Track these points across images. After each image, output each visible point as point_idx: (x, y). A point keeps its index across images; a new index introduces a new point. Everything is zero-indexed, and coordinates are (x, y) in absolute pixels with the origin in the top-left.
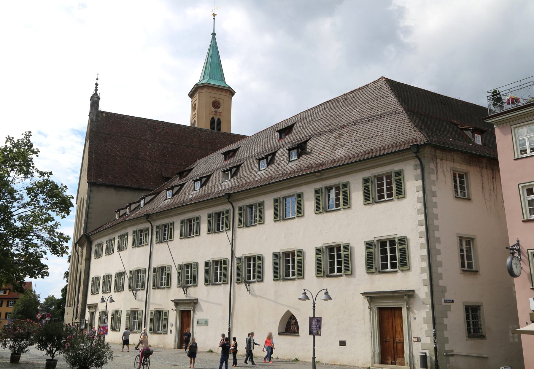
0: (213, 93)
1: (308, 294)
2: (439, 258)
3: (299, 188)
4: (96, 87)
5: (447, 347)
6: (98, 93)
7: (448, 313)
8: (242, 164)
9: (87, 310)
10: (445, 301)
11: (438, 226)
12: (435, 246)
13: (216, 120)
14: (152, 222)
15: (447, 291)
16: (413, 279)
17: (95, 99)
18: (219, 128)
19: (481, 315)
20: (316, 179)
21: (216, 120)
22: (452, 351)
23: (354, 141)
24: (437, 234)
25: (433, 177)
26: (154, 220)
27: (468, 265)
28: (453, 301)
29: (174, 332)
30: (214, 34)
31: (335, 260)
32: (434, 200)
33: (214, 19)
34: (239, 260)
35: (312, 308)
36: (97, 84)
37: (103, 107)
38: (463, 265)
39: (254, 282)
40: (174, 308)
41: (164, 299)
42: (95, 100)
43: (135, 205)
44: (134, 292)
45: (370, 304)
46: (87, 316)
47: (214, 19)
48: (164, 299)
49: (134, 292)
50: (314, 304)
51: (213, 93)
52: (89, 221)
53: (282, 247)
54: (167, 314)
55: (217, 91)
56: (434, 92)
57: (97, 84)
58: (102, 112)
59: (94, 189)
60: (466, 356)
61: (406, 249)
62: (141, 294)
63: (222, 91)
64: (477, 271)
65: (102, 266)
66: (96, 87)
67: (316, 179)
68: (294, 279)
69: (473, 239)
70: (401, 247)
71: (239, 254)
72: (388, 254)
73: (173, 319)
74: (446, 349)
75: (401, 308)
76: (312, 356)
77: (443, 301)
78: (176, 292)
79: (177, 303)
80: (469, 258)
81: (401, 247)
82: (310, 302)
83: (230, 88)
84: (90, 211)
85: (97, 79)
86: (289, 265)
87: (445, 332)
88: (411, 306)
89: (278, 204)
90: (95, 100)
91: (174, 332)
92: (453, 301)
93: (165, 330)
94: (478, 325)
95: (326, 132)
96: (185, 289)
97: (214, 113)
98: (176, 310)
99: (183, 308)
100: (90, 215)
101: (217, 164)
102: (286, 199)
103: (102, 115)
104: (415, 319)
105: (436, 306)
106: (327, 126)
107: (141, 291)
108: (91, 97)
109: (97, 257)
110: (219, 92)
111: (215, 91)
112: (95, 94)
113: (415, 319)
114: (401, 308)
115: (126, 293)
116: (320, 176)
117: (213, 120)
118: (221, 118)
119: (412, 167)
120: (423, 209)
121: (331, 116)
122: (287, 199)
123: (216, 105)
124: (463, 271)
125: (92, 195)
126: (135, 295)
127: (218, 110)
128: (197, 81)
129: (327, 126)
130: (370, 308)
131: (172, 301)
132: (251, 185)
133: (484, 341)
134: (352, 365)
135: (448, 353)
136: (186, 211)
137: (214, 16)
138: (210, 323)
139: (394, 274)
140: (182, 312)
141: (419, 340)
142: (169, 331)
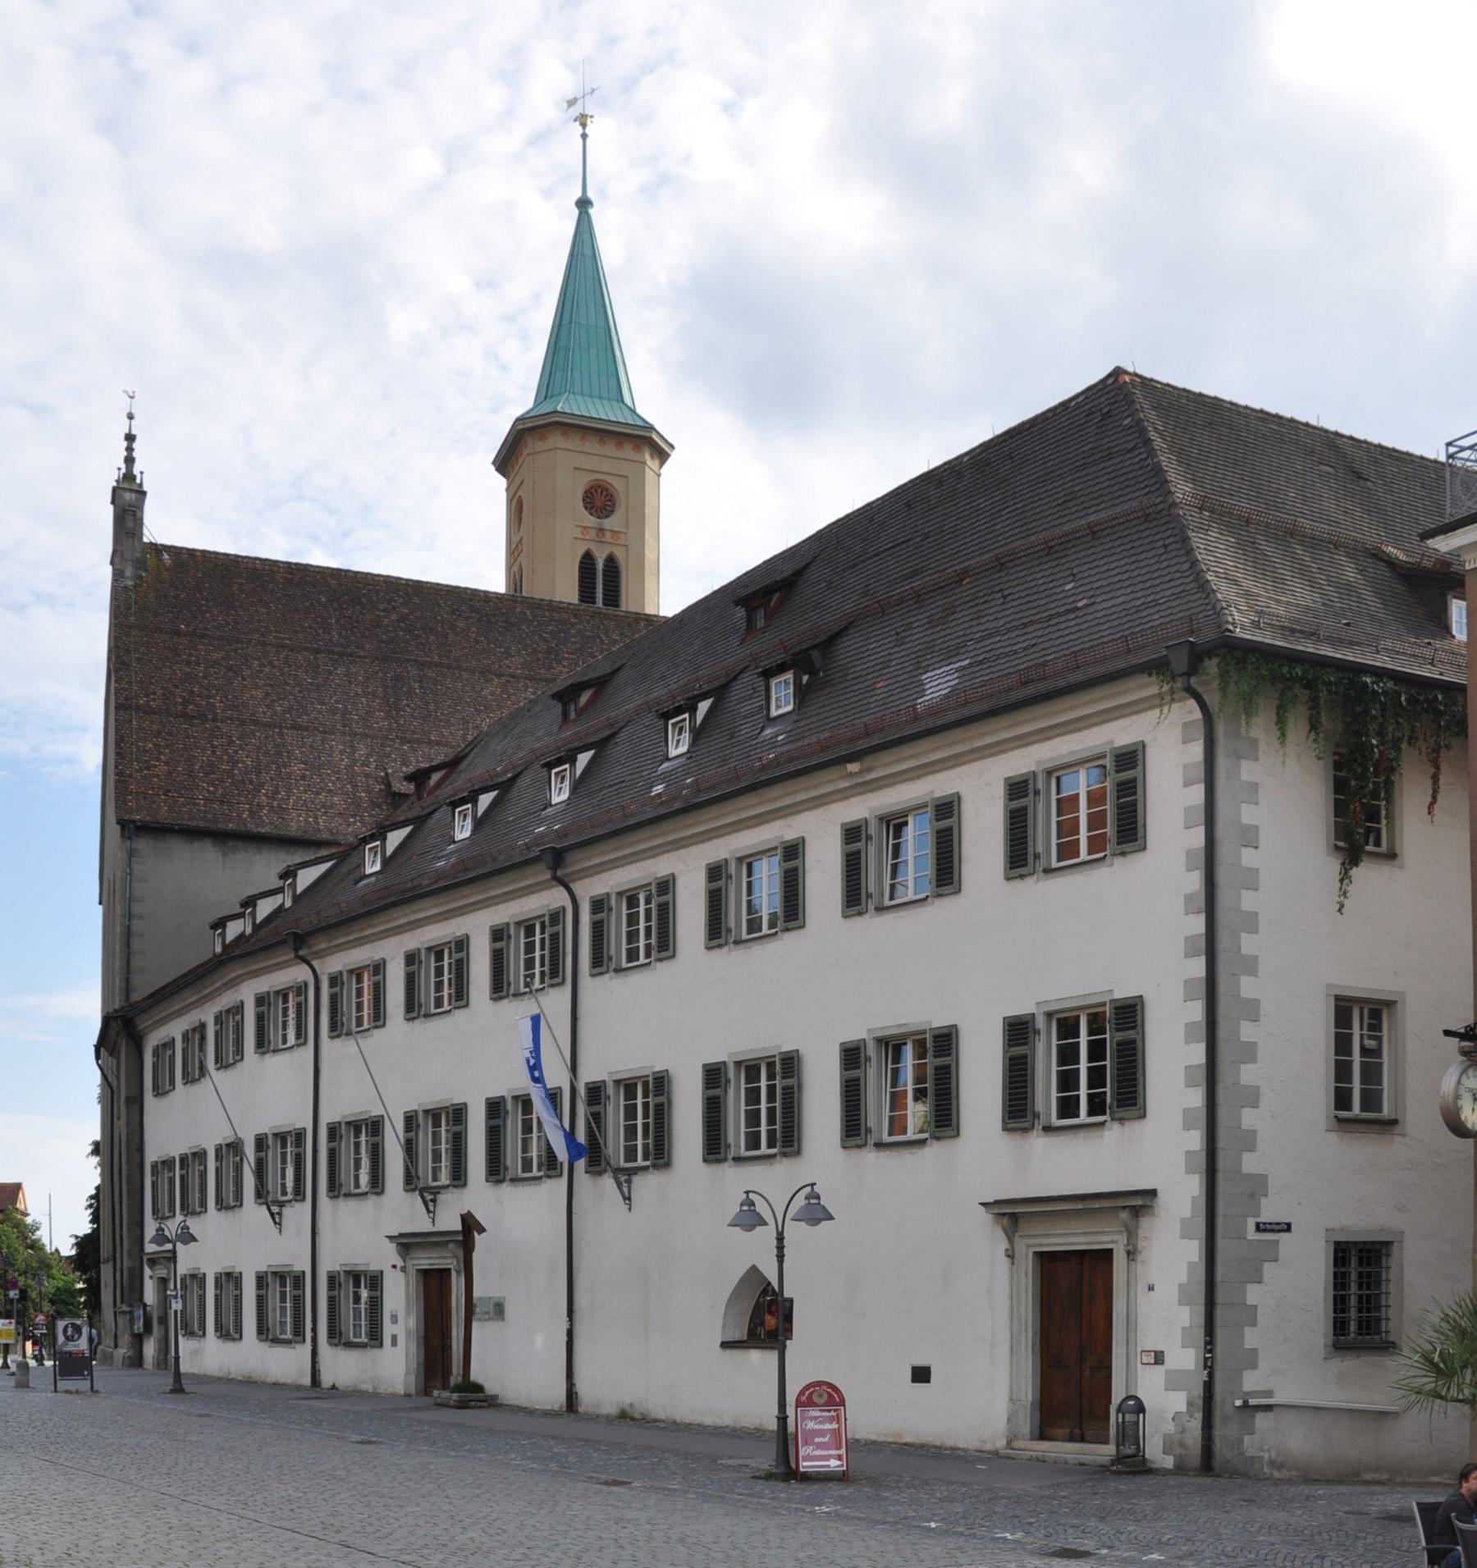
0: (578, 447)
1: (761, 1207)
2: (1248, 1074)
3: (790, 820)
4: (130, 449)
5: (1251, 1381)
6: (136, 471)
7: (1268, 1268)
8: (614, 735)
9: (147, 1272)
10: (1259, 1228)
11: (1256, 958)
12: (1236, 1032)
13: (600, 565)
14: (315, 963)
15: (1271, 1191)
16: (1151, 1150)
17: (128, 496)
18: (613, 596)
19: (1393, 1273)
20: (846, 784)
21: (600, 565)
22: (1269, 1394)
23: (991, 635)
24: (1248, 987)
25: (1249, 771)
26: (319, 955)
27: (1359, 1097)
28: (1288, 1228)
29: (401, 1340)
30: (584, 204)
31: (907, 1081)
32: (1248, 857)
33: (584, 136)
34: (596, 1092)
35: (786, 1251)
36: (130, 438)
37: (164, 526)
38: (1342, 1099)
39: (646, 1168)
40: (399, 1263)
41: (363, 1231)
42: (128, 501)
43: (270, 900)
44: (275, 1209)
45: (1011, 1240)
46: (150, 1295)
47: (584, 136)
48: (363, 1231)
49: (275, 1209)
50: (780, 1238)
51: (578, 447)
52: (136, 962)
53: (729, 1044)
54: (375, 1281)
55: (602, 442)
56: (1332, 428)
57: (130, 438)
58: (157, 549)
59: (143, 845)
60: (1318, 1408)
61: (1139, 1042)
62: (297, 1215)
63: (620, 445)
64: (1393, 1122)
65: (179, 1123)
66: (130, 449)
67: (846, 784)
68: (774, 1156)
69: (1390, 1004)
70: (1120, 1036)
71: (589, 1073)
72: (1089, 1060)
73: (399, 1298)
74: (1247, 1387)
75: (1111, 1251)
76: (776, 1412)
77: (1251, 1224)
78: (400, 1210)
79: (407, 1244)
80: (1372, 1074)
81: (1120, 1036)
82: (768, 1233)
83: (652, 428)
84: (137, 926)
85: (131, 417)
86: (757, 1104)
87: (1248, 1331)
88: (1141, 1245)
89: (722, 883)
90: (128, 501)
91: (401, 1340)
92: (1288, 1228)
93: (375, 1337)
94: (1378, 1308)
95: (901, 601)
96: (429, 1197)
97: (593, 535)
98: (403, 1269)
99: (428, 1260)
100: (135, 943)
101: (539, 739)
102: (750, 866)
103: (160, 560)
104: (1151, 1288)
105: (1221, 1243)
106: (907, 577)
107: (297, 1205)
108: (115, 490)
109: (159, 1092)
110: (610, 449)
111: (592, 445)
112: (129, 477)
113: (1151, 1288)
114: (1111, 1251)
115: (253, 1213)
116: (861, 772)
117: (587, 562)
118: (620, 554)
119: (1176, 733)
120: (1202, 896)
121: (926, 536)
122: (756, 865)
123: (600, 500)
124: (1339, 1120)
125: (136, 867)
126: (277, 1219)
127: (607, 523)
128: (519, 410)
129: (907, 577)
130: (1010, 1255)
131: (390, 1237)
132: (633, 815)
133: (1388, 1361)
134: (950, 1443)
135: (1252, 1402)
136: (419, 916)
137: (584, 125)
138: (509, 1310)
139: (1094, 1133)
140: (426, 1274)
141: (1159, 1358)
142: (387, 1340)
